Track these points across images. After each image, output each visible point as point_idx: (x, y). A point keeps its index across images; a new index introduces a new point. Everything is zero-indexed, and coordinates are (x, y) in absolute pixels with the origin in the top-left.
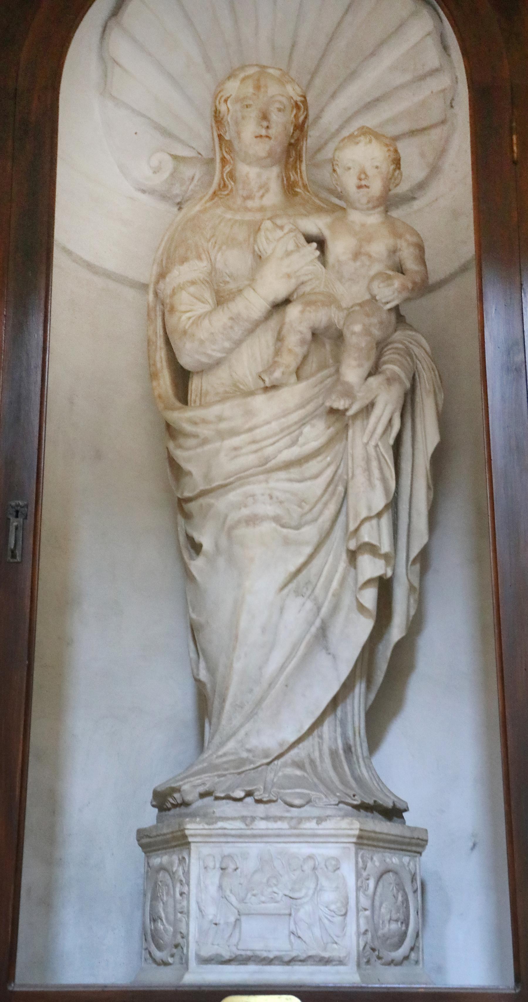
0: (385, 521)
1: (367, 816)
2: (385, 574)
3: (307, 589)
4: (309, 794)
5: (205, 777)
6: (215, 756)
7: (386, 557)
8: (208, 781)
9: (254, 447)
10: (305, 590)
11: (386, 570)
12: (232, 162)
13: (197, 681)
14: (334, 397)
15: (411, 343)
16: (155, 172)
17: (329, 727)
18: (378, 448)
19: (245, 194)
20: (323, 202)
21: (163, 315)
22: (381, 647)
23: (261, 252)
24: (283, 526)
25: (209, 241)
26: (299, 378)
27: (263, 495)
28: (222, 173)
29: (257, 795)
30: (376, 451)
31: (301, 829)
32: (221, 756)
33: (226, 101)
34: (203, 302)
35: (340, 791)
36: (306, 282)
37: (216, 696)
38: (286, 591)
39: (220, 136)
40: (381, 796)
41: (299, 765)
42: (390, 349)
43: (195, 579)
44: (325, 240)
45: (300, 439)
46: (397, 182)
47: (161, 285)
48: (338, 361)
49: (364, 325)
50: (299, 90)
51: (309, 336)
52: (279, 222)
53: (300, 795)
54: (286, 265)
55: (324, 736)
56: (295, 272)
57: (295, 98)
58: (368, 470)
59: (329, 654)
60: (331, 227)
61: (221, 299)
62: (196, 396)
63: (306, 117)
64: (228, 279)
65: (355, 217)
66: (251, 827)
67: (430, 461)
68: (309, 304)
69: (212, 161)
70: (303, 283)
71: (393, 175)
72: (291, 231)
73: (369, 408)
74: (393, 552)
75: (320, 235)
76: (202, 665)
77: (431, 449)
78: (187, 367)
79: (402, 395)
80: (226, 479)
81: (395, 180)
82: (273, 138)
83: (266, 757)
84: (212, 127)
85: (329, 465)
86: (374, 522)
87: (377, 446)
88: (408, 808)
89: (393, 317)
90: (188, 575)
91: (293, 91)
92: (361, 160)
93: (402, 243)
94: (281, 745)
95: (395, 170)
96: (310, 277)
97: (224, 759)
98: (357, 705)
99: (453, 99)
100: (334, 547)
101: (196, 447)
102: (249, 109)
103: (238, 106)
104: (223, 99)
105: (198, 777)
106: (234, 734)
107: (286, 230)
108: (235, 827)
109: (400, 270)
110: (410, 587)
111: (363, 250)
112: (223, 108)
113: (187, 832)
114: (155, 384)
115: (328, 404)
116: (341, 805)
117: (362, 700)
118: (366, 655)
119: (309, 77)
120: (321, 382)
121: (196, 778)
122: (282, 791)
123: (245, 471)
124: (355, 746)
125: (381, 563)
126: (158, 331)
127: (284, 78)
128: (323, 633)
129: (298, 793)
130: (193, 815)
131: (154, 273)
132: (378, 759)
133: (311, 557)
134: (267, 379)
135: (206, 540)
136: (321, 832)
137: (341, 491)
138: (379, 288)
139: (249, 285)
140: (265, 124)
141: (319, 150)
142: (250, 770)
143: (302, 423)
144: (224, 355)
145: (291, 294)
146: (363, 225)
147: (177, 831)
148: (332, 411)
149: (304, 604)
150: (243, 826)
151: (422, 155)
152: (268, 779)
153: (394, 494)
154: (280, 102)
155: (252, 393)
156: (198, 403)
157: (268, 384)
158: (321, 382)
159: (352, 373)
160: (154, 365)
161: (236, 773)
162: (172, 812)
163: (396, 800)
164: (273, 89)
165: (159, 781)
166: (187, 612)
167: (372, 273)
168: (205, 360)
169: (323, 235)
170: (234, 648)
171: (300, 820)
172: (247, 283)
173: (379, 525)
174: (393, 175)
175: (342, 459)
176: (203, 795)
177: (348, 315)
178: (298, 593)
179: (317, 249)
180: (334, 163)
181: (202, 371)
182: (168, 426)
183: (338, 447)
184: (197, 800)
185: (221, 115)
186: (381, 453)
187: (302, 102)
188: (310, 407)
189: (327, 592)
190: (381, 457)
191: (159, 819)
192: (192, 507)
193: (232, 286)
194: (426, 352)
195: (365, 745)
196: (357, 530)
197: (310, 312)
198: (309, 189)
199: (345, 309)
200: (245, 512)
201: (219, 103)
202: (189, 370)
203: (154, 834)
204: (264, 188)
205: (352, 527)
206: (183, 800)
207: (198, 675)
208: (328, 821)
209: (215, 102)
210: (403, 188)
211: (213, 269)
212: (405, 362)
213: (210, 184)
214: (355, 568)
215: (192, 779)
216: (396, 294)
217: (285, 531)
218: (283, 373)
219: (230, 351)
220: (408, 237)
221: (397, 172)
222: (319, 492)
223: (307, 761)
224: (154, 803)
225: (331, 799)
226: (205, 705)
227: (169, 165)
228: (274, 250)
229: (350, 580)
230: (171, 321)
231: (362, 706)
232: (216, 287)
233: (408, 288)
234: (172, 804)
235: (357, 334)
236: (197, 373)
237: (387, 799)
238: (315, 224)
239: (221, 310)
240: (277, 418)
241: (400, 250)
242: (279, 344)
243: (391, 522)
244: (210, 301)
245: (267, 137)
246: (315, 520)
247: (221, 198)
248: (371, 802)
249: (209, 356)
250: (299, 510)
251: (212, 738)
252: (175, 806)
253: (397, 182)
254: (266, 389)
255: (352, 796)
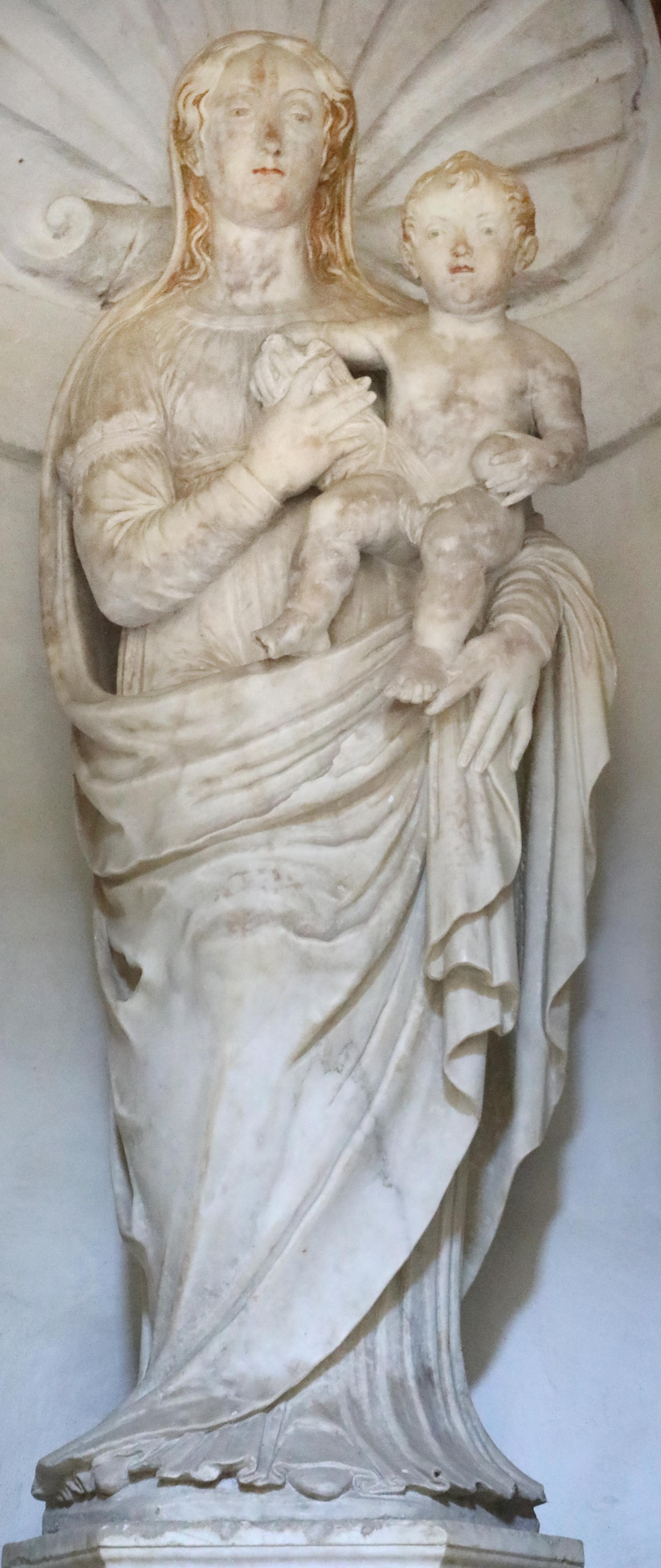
0: (501, 921)
1: (462, 1516)
2: (501, 1027)
3: (347, 1057)
4: (348, 1471)
5: (139, 1438)
6: (161, 1395)
7: (503, 994)
8: (145, 1446)
9: (246, 777)
10: (342, 1058)
11: (502, 1020)
12: (207, 218)
13: (128, 1241)
14: (402, 680)
15: (555, 571)
16: (56, 236)
17: (388, 1332)
18: (488, 779)
19: (231, 279)
20: (382, 293)
21: (71, 514)
22: (491, 1169)
23: (260, 394)
24: (300, 933)
25: (161, 373)
26: (333, 640)
27: (261, 871)
28: (188, 240)
29: (245, 1476)
30: (484, 784)
31: (330, 1545)
32: (174, 1395)
33: (197, 102)
34: (150, 493)
35: (409, 1464)
36: (348, 454)
37: (166, 1273)
38: (304, 1061)
39: (185, 169)
40: (492, 1473)
41: (329, 1412)
42: (513, 582)
43: (128, 1038)
44: (386, 368)
45: (335, 761)
46: (528, 258)
47: (68, 459)
48: (410, 604)
49: (462, 537)
50: (339, 82)
51: (354, 559)
52: (298, 337)
53: (330, 1475)
54: (312, 420)
55: (378, 1351)
56: (329, 435)
57: (331, 97)
58: (468, 820)
59: (390, 1186)
60: (398, 345)
61: (183, 487)
62: (134, 674)
63: (352, 132)
64: (197, 446)
65: (446, 326)
66: (230, 1542)
67: (591, 800)
68: (353, 497)
69: (168, 212)
70: (344, 455)
71: (520, 246)
72: (321, 354)
73: (470, 699)
74: (516, 980)
75: (377, 361)
76: (138, 1208)
77: (592, 776)
78: (115, 619)
79: (535, 672)
80: (189, 840)
81: (525, 254)
82: (288, 172)
83: (263, 1396)
84: (169, 150)
85: (391, 811)
86: (479, 923)
87: (485, 773)
88: (544, 1497)
89: (519, 521)
90: (113, 1030)
91: (327, 82)
92: (454, 219)
93: (537, 377)
94: (293, 1370)
95: (524, 235)
96: (358, 443)
97: (180, 1401)
98: (442, 1289)
99: (638, 94)
100: (401, 972)
101: (132, 777)
102: (241, 118)
103: (220, 113)
104: (191, 99)
105: (128, 1438)
106: (199, 1350)
107: (312, 352)
108: (198, 1543)
109: (534, 429)
110: (550, 1049)
111: (460, 391)
112: (191, 116)
113: (104, 1553)
114: (52, 651)
115: (390, 693)
116: (411, 1494)
117: (454, 1276)
118: (462, 1190)
119: (359, 51)
120: (378, 648)
121: (123, 1440)
122: (294, 1466)
123: (225, 826)
124: (440, 1371)
125: (493, 1004)
126: (60, 548)
127: (312, 55)
128: (377, 1144)
129: (325, 1470)
130: (116, 1518)
131: (53, 432)
132: (488, 1396)
133: (355, 994)
134: (271, 645)
135: (150, 965)
136: (371, 1551)
137: (414, 863)
138: (490, 464)
139: (239, 460)
140: (272, 146)
141: (379, 188)
142: (230, 1422)
143: (340, 729)
144: (189, 595)
145: (322, 477)
146: (461, 342)
147: (83, 1552)
148: (398, 706)
149: (340, 1087)
150: (216, 1540)
151: (579, 200)
152: (266, 1441)
153: (520, 866)
154: (305, 105)
155: (241, 671)
156: (136, 691)
157: (273, 653)
158: (378, 648)
159: (438, 631)
160: (52, 613)
161: (203, 1430)
162: (75, 1509)
163: (519, 1479)
164: (289, 80)
165: (50, 1444)
166: (109, 1101)
167: (479, 434)
168: (151, 605)
169: (381, 358)
170: (202, 1176)
171: (330, 1525)
172: (233, 454)
173: (488, 931)
174: (520, 246)
175: (417, 800)
176: (136, 1476)
177: (432, 518)
178: (329, 1066)
179: (371, 388)
180: (407, 222)
181: (145, 627)
182: (77, 734)
183: (410, 776)
184: (125, 1486)
185: (187, 130)
186: (493, 785)
187: (343, 102)
188: (355, 699)
189: (386, 1064)
190: (495, 796)
191: (50, 1527)
192: (123, 894)
193: (205, 460)
194: (582, 584)
195: (459, 1368)
196: (445, 940)
197: (357, 514)
198: (356, 267)
199: (426, 505)
200: (226, 905)
201: (184, 106)
202: (119, 623)
203: (38, 1555)
204: (270, 269)
205: (436, 936)
206: (97, 1485)
207: (130, 1228)
208: (385, 1529)
209: (176, 106)
210: (543, 262)
211: (168, 428)
212: (539, 606)
213: (167, 258)
214: (442, 1013)
215: (115, 1443)
216: (524, 477)
217: (304, 942)
218: (303, 633)
219: (199, 589)
220: (549, 364)
221: (529, 238)
222: (371, 865)
223: (343, 1404)
224: (39, 1491)
225: (391, 1483)
226: (142, 1288)
227: (85, 221)
228: (288, 392)
229: (432, 1038)
230: (86, 531)
231: (455, 1287)
232: (174, 463)
233: (548, 465)
234: (74, 1493)
235: (449, 554)
236: (135, 629)
237: (502, 1480)
238: (367, 341)
239: (184, 508)
240: (291, 720)
241: (533, 390)
242: (296, 575)
243: (513, 924)
244: (163, 490)
245: (277, 171)
246: (364, 920)
247: (184, 288)
248: (471, 1487)
249: (160, 598)
250: (334, 899)
251: (157, 1357)
252: (81, 1497)
253: (528, 258)
254: (270, 663)
255: (433, 1474)
